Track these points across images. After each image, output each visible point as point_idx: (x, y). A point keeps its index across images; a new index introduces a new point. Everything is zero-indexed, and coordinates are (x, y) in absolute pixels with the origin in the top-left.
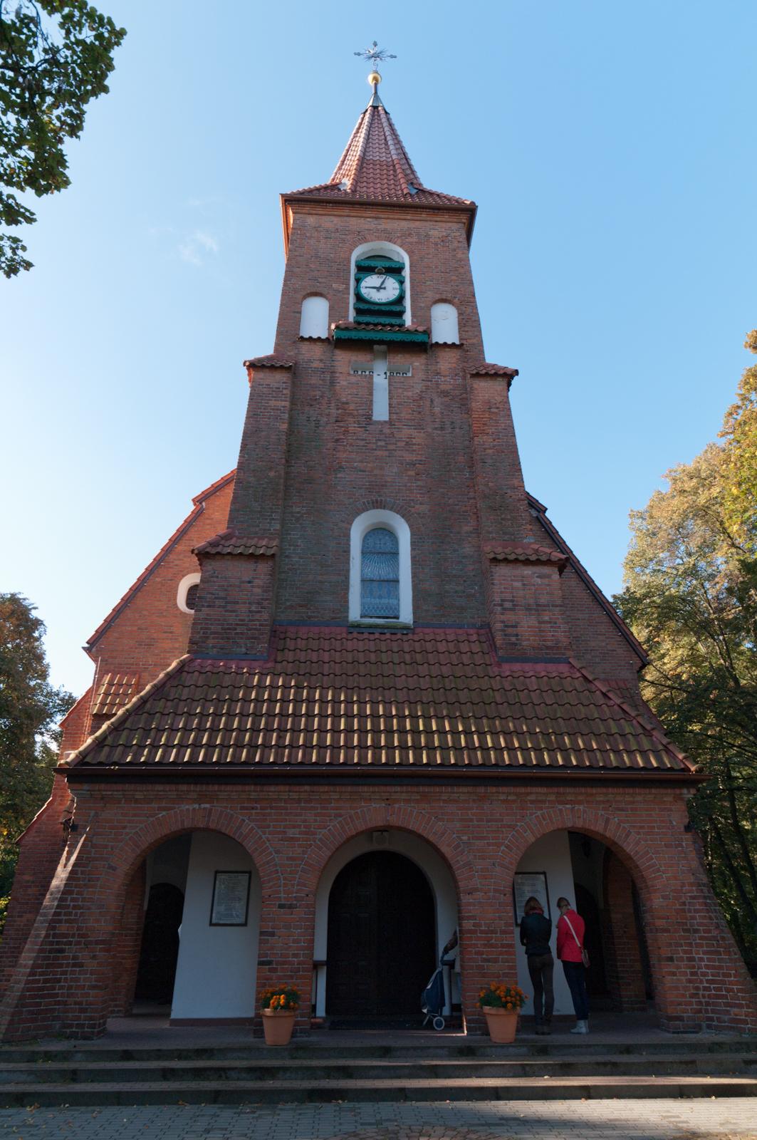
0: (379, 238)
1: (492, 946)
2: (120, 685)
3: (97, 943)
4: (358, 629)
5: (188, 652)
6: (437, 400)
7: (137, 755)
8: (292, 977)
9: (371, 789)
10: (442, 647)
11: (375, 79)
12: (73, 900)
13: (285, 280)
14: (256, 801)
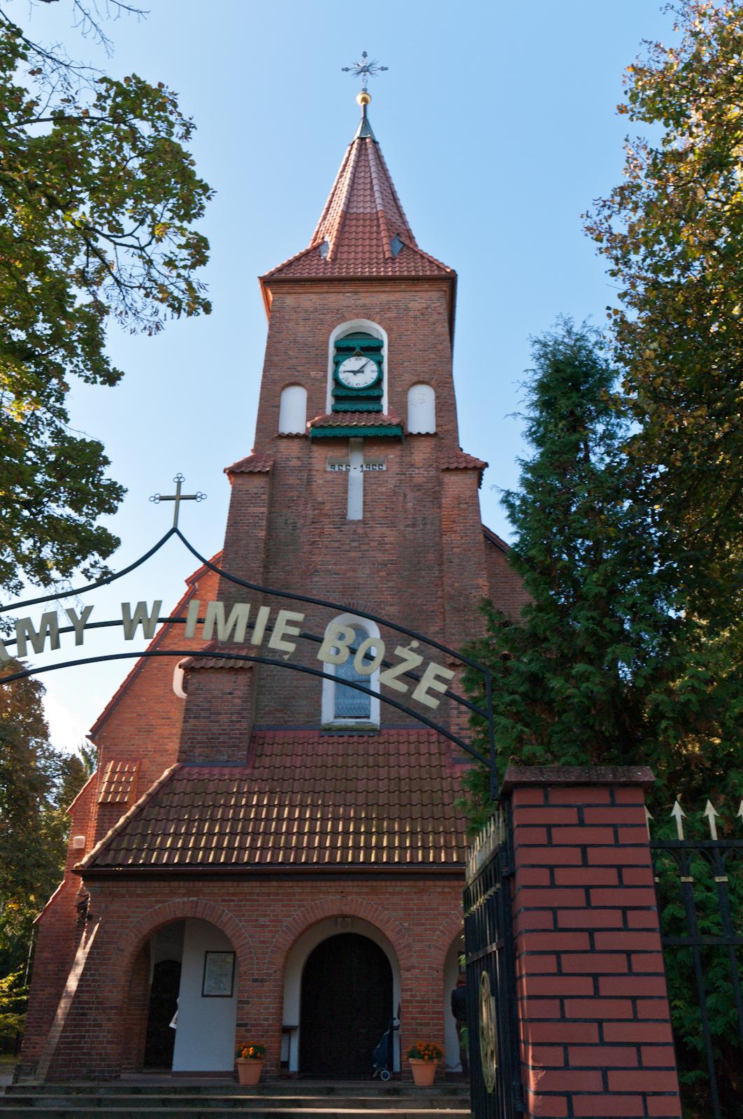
0: (357, 316)
1: (424, 1013)
2: (122, 772)
3: (112, 1008)
4: (329, 733)
5: (178, 761)
6: (410, 496)
7: (136, 858)
8: (263, 1036)
9: (328, 884)
10: (403, 749)
11: (364, 100)
12: (91, 975)
13: (265, 371)
14: (234, 895)
